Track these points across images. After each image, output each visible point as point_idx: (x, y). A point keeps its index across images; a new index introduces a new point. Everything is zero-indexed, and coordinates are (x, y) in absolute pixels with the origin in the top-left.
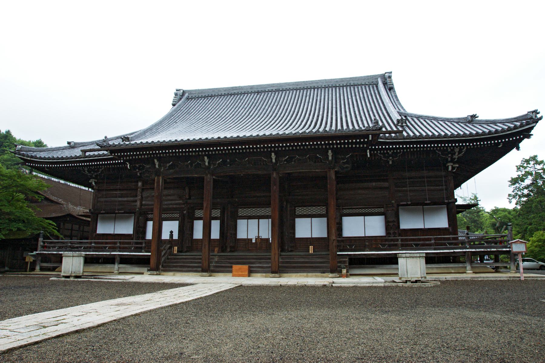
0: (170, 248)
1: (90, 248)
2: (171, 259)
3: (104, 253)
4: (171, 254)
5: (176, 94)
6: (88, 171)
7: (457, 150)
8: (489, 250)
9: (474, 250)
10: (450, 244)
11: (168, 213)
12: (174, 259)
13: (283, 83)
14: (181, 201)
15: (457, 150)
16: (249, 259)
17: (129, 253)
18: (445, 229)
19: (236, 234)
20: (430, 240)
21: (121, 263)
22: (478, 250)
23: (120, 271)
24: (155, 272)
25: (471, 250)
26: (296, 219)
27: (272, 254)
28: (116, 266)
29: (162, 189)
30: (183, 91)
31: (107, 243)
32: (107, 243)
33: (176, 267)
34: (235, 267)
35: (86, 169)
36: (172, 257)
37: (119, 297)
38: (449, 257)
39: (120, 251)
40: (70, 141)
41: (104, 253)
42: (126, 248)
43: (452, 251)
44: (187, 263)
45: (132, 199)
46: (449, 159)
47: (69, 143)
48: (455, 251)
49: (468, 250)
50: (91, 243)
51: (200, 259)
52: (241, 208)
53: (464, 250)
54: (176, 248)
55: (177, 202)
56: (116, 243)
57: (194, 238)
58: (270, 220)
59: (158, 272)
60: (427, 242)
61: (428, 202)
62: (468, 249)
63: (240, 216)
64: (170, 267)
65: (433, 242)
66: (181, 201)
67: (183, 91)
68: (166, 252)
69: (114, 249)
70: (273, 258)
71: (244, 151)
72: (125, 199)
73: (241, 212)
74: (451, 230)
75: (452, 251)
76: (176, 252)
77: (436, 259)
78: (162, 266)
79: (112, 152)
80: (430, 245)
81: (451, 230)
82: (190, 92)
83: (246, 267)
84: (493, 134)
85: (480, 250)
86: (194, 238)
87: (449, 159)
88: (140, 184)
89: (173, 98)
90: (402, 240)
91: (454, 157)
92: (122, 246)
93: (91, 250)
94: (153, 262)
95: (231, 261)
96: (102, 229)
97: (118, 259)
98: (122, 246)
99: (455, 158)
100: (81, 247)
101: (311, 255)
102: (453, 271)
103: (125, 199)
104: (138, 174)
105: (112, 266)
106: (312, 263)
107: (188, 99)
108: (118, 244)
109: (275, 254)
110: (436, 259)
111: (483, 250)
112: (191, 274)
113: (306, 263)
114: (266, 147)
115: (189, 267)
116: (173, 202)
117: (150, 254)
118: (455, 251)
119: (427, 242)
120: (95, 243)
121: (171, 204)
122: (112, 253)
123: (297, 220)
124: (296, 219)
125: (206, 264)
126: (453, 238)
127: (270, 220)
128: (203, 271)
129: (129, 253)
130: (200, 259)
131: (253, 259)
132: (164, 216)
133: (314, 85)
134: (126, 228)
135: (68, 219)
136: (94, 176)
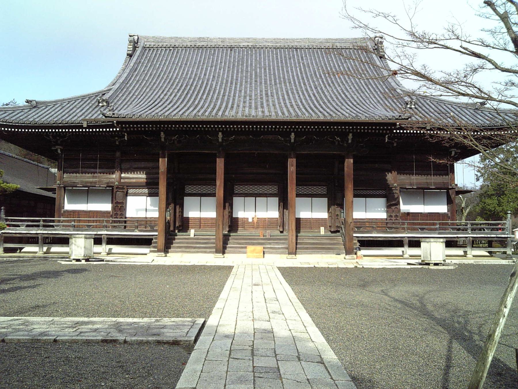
10: (453, 229)
11: (153, 188)
18: (107, 212)
26: (185, 198)
34: (250, 248)
37: (332, 268)
40: (30, 99)
47: (27, 102)
52: (236, 185)
57: (184, 216)
61: (433, 187)
63: (237, 194)
65: (438, 226)
71: (366, 131)
73: (189, 189)
74: (449, 215)
80: (436, 229)
81: (449, 215)
83: (260, 248)
86: (184, 216)
88: (118, 154)
90: (472, 224)
95: (240, 241)
104: (117, 143)
113: (317, 244)
114: (378, 129)
115: (195, 248)
123: (186, 198)
124: (185, 198)
126: (451, 223)
133: (296, 44)
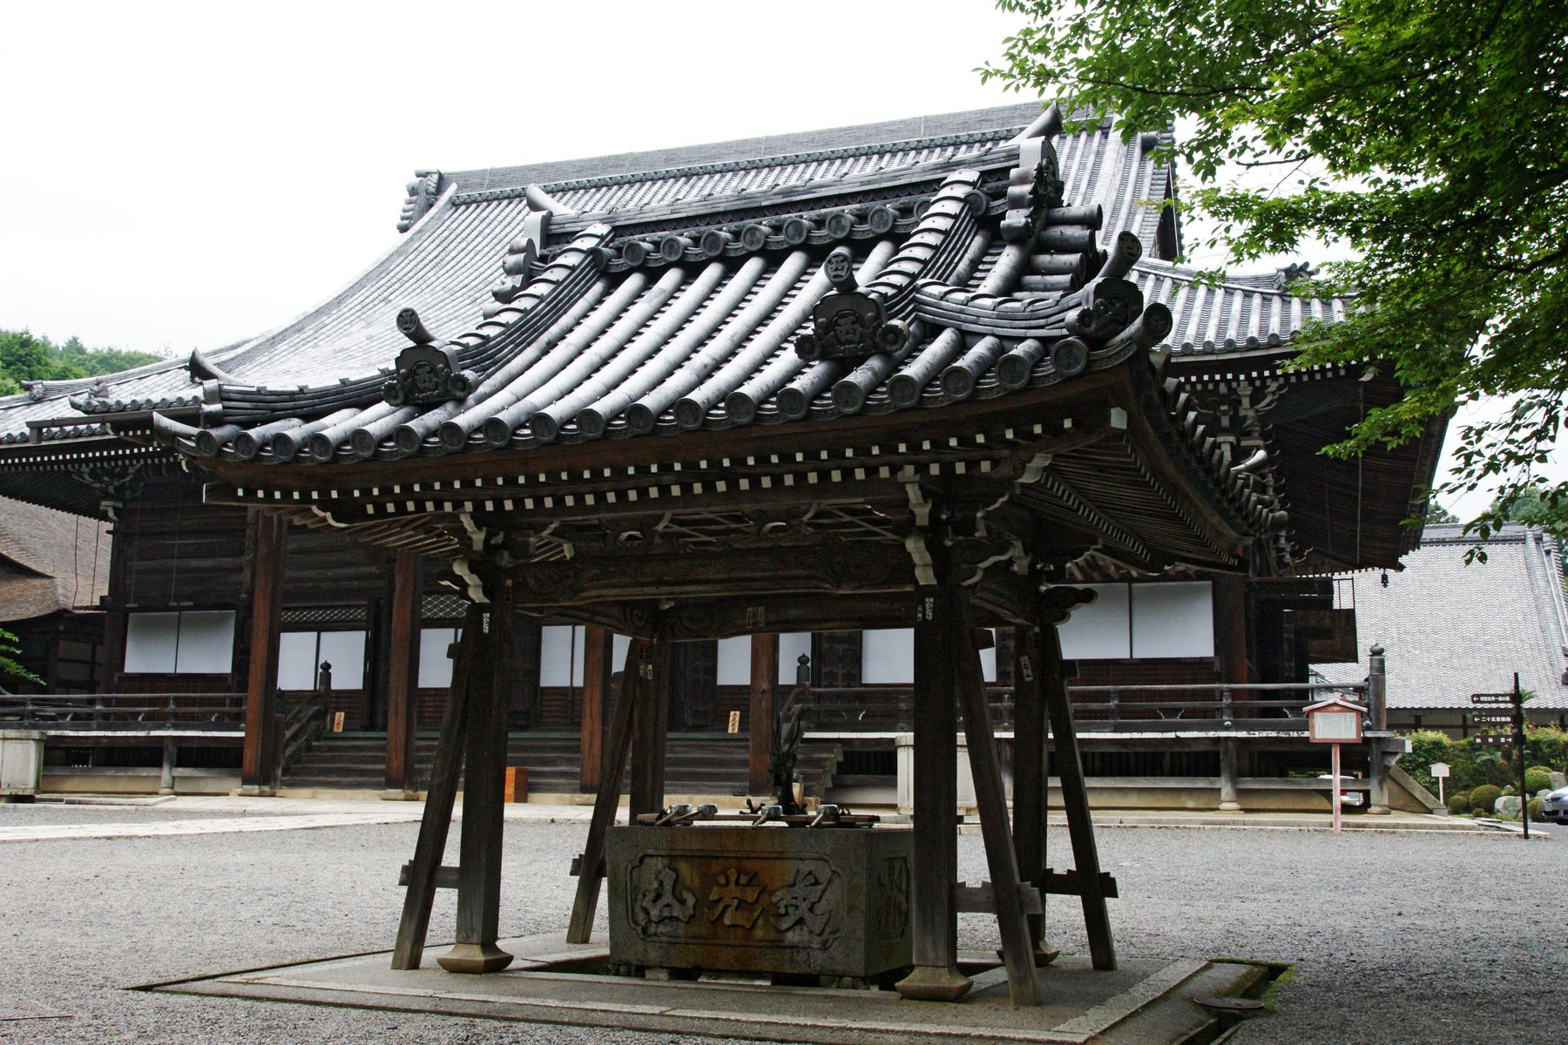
0: (320, 715)
1: (89, 717)
2: (319, 748)
3: (131, 734)
4: (323, 733)
5: (413, 191)
6: (90, 475)
7: (1245, 390)
8: (1295, 734)
9: (1243, 734)
11: (335, 607)
12: (330, 749)
13: (777, 138)
14: (373, 569)
15: (1245, 390)
16: (544, 749)
17: (200, 734)
18: (1200, 662)
19: (535, 672)
20: (1104, 697)
21: (180, 763)
22: (1257, 734)
23: (177, 789)
24: (256, 789)
25: (1233, 734)
27: (585, 733)
28: (166, 773)
29: (280, 534)
30: (441, 177)
31: (140, 703)
32: (140, 703)
33: (326, 772)
35: (84, 469)
36: (322, 743)
38: (1162, 754)
39: (176, 728)
41: (131, 734)
42: (193, 717)
43: (1171, 735)
44: (363, 760)
45: (228, 561)
46: (1225, 422)
48: (1182, 735)
49: (1223, 734)
50: (91, 702)
51: (382, 749)
53: (1211, 734)
54: (340, 716)
55: (363, 570)
56: (165, 702)
58: (581, 631)
59: (266, 789)
60: (1094, 706)
62: (1227, 729)
64: (308, 772)
65: (1113, 704)
66: (373, 569)
67: (441, 177)
68: (303, 728)
69: (156, 720)
70: (586, 747)
72: (208, 563)
74: (1217, 666)
75: (1171, 735)
76: (338, 729)
77: (1167, 762)
78: (285, 772)
79: (117, 427)
80: (1104, 714)
81: (1217, 666)
82: (465, 179)
84: (1236, 350)
85: (1264, 734)
87: (1225, 422)
89: (404, 206)
91: (1242, 413)
92: (183, 709)
93: (94, 723)
94: (250, 756)
96: (138, 661)
97: (171, 750)
98: (183, 709)
99: (1245, 418)
100: (64, 716)
101: (732, 739)
102: (1190, 804)
103: (208, 563)
105: (152, 772)
106: (722, 763)
107: (455, 204)
108: (172, 707)
109: (592, 733)
110: (1167, 762)
111: (1274, 734)
112: (360, 793)
115: (362, 773)
116: (353, 570)
117: (242, 734)
118: (1182, 735)
119: (1094, 706)
120: (106, 702)
121: (348, 578)
122: (153, 733)
125: (397, 763)
127: (581, 631)
128: (391, 783)
129: (200, 734)
130: (382, 749)
131: (557, 749)
132: (287, 616)
134: (210, 656)
135: (62, 628)
136: (111, 490)
